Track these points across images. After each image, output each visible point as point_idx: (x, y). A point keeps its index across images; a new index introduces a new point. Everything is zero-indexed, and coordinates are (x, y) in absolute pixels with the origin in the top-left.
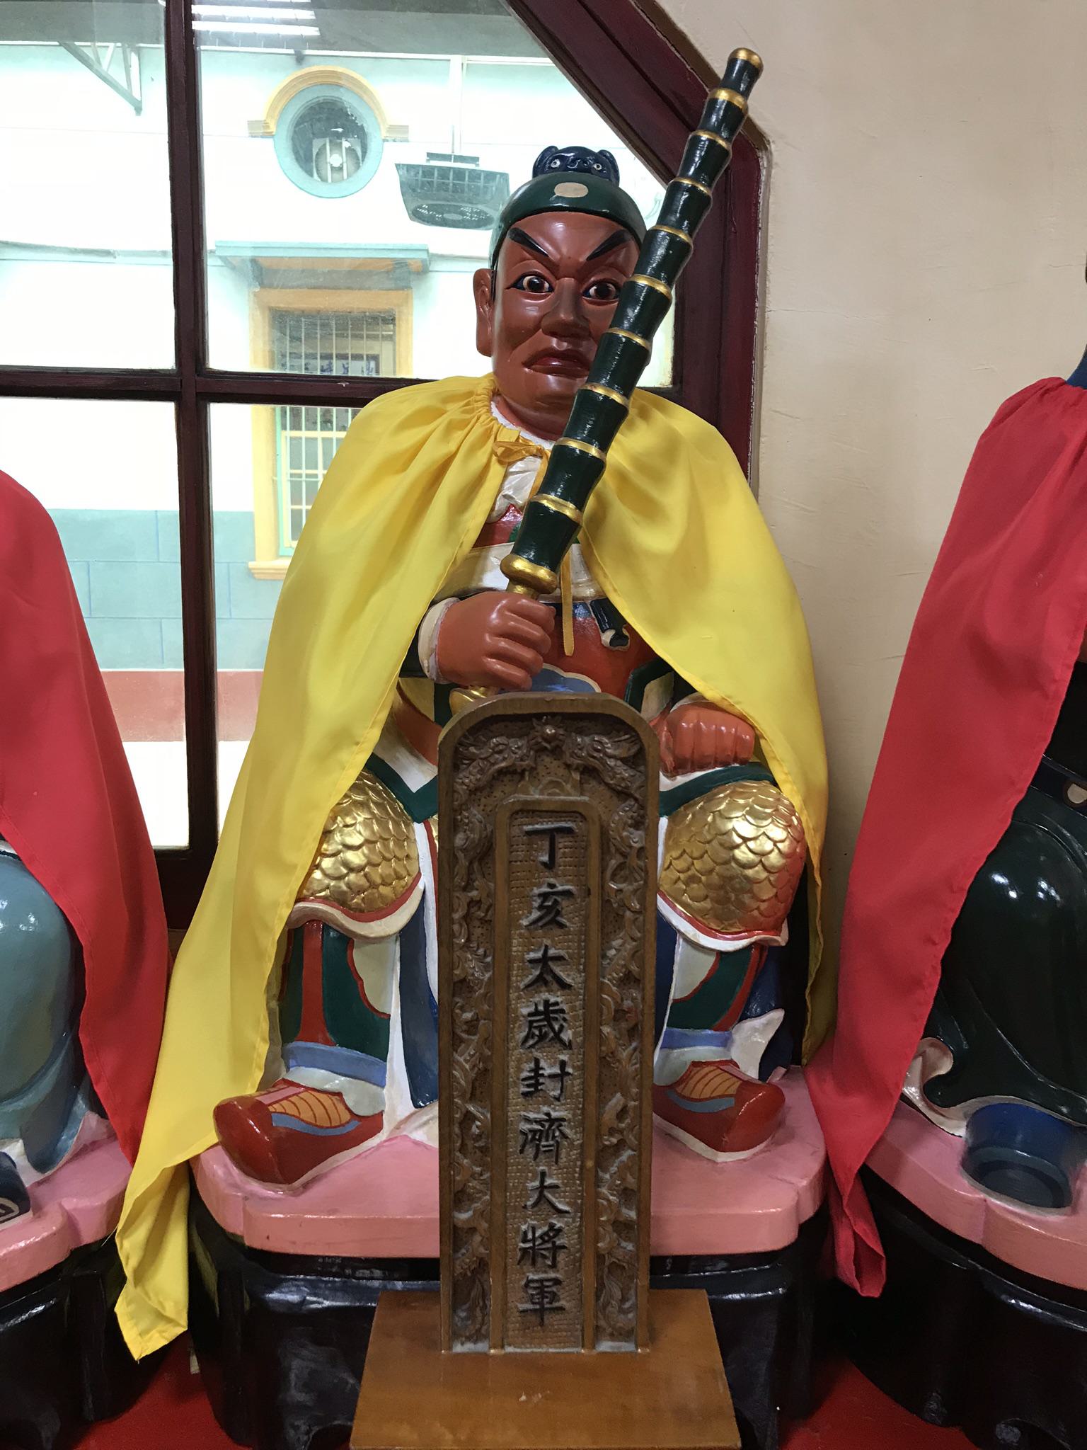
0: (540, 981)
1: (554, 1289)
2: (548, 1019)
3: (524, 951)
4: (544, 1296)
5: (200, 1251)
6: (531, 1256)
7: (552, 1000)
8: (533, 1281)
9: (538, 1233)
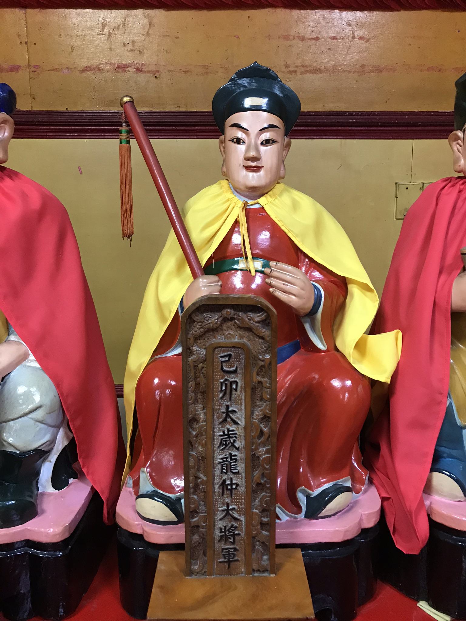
0: (225, 420)
1: (235, 553)
2: (229, 437)
3: (219, 457)
7: (233, 453)
8: (226, 549)
9: (227, 529)
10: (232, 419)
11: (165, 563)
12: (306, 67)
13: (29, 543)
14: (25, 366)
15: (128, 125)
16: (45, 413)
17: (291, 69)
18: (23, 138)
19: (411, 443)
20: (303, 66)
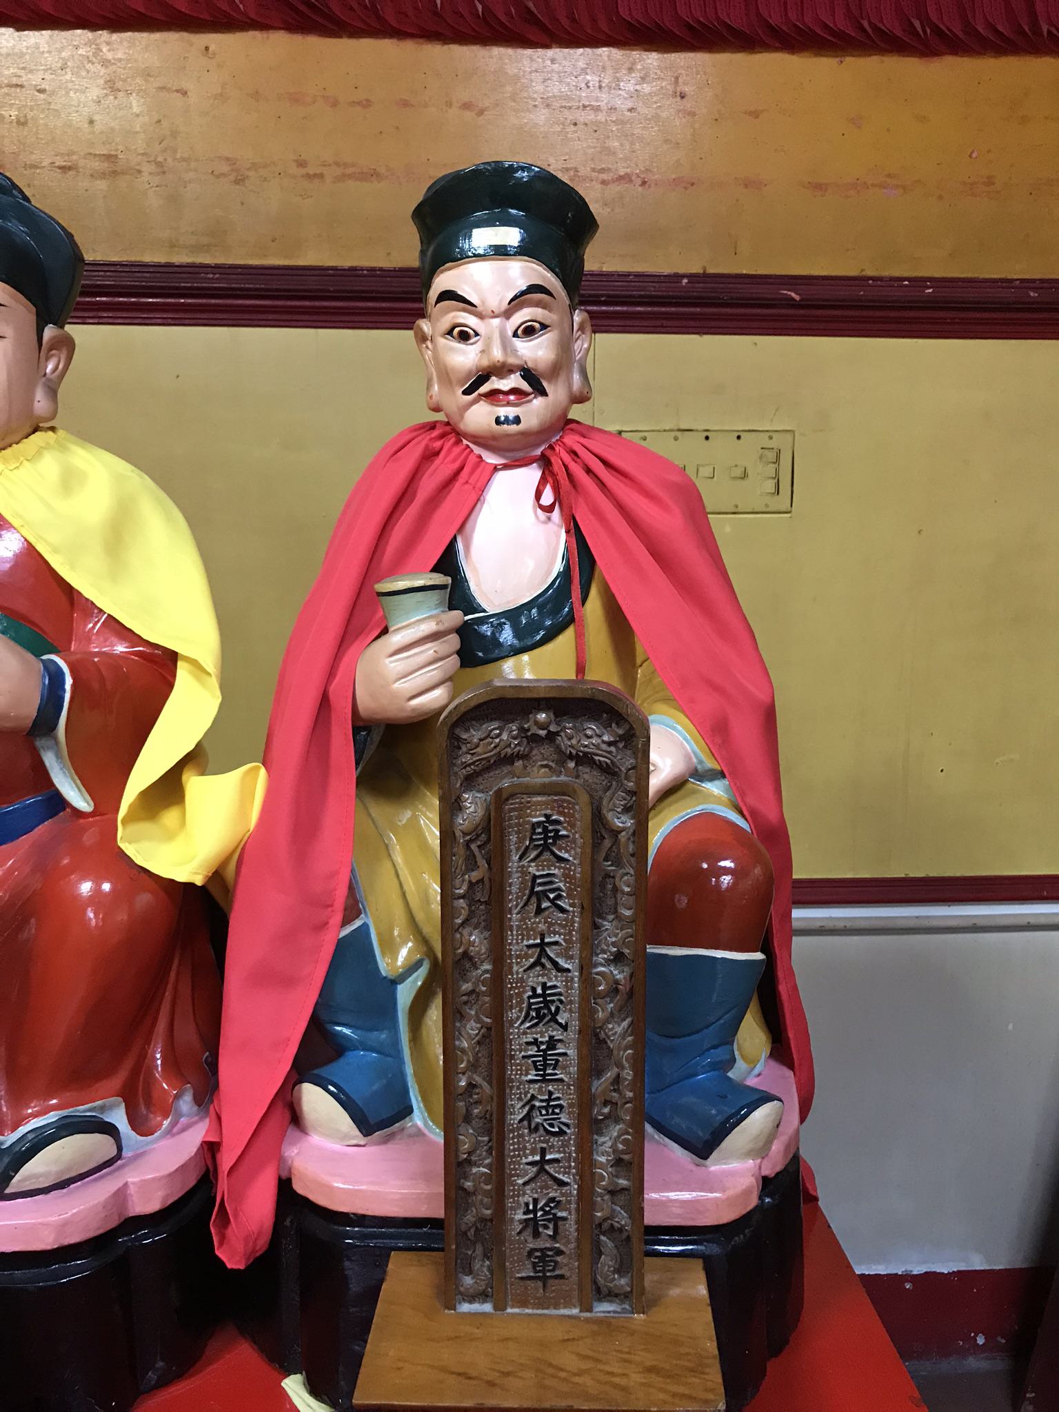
0: (537, 963)
4: (544, 1261)
8: (536, 1250)
11: (406, 1277)
12: (346, 165)
17: (311, 170)
19: (262, 1021)
20: (337, 164)
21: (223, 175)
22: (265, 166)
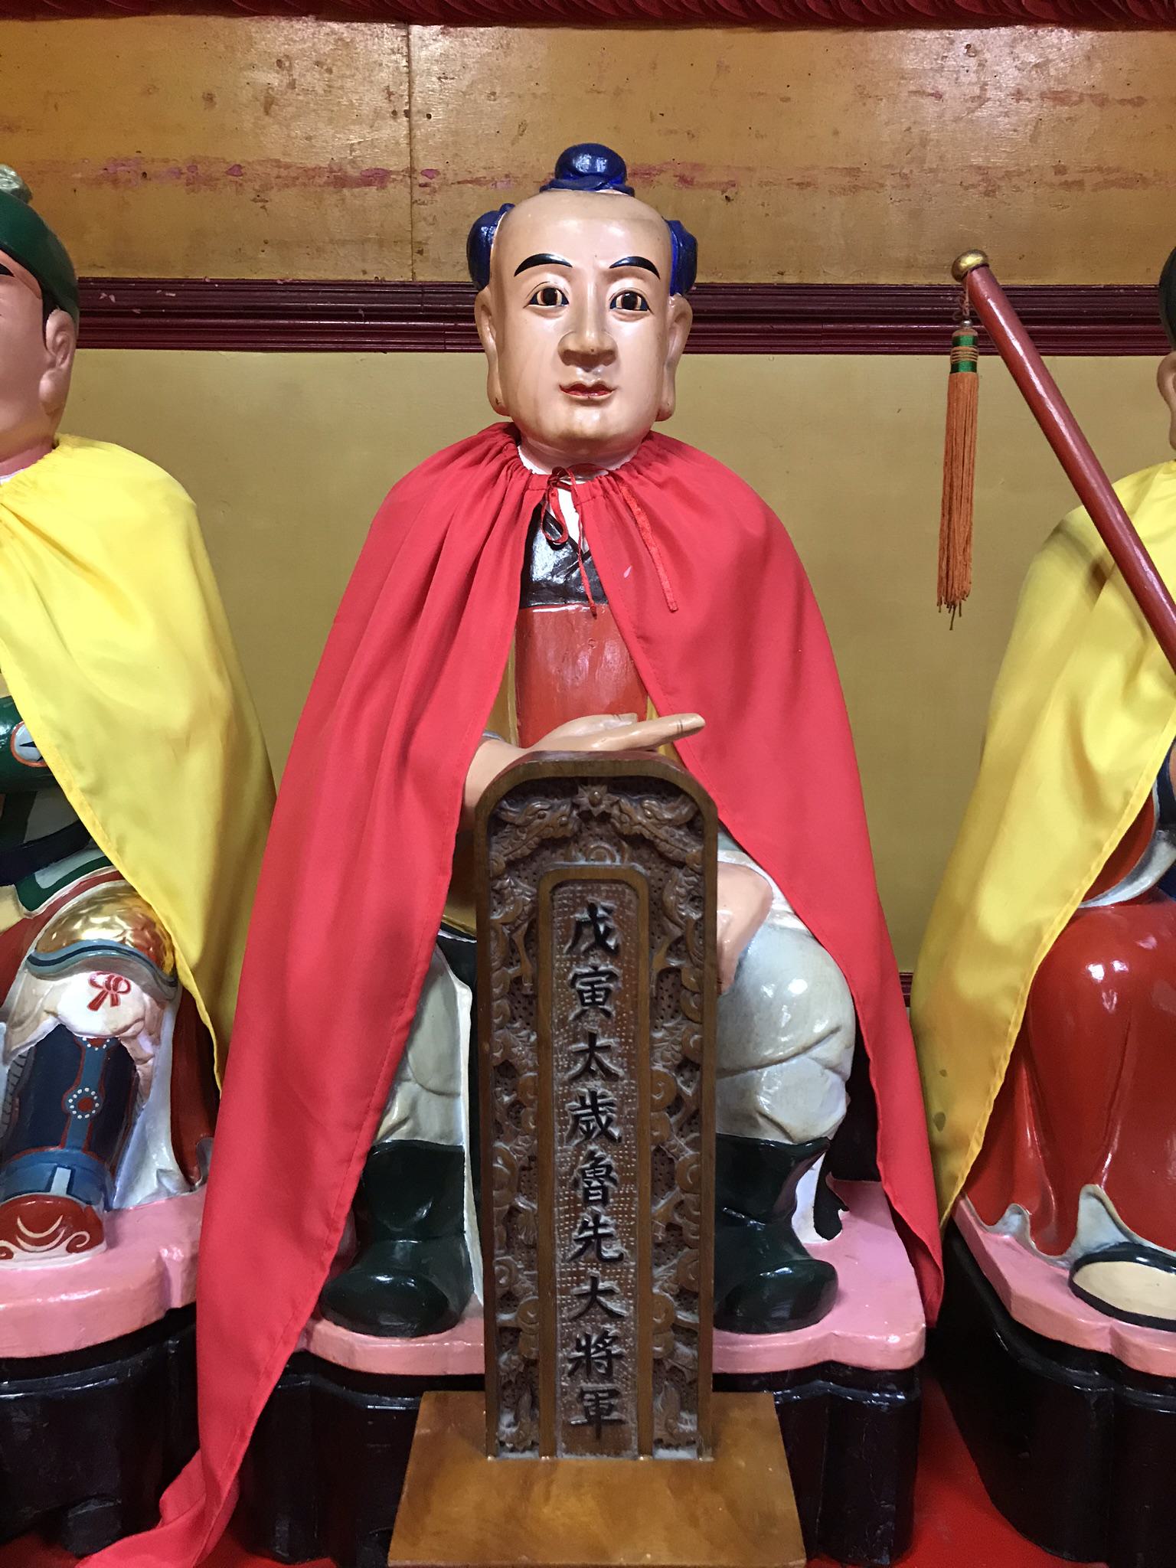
5: (1025, 1099)
6: (583, 1366)
10: (600, 1064)
12: (1110, 171)
13: (829, 1369)
14: (773, 926)
15: (975, 322)
16: (843, 1046)
18: (385, 351)
20: (1100, 169)
21: (973, 186)
22: (1020, 174)
